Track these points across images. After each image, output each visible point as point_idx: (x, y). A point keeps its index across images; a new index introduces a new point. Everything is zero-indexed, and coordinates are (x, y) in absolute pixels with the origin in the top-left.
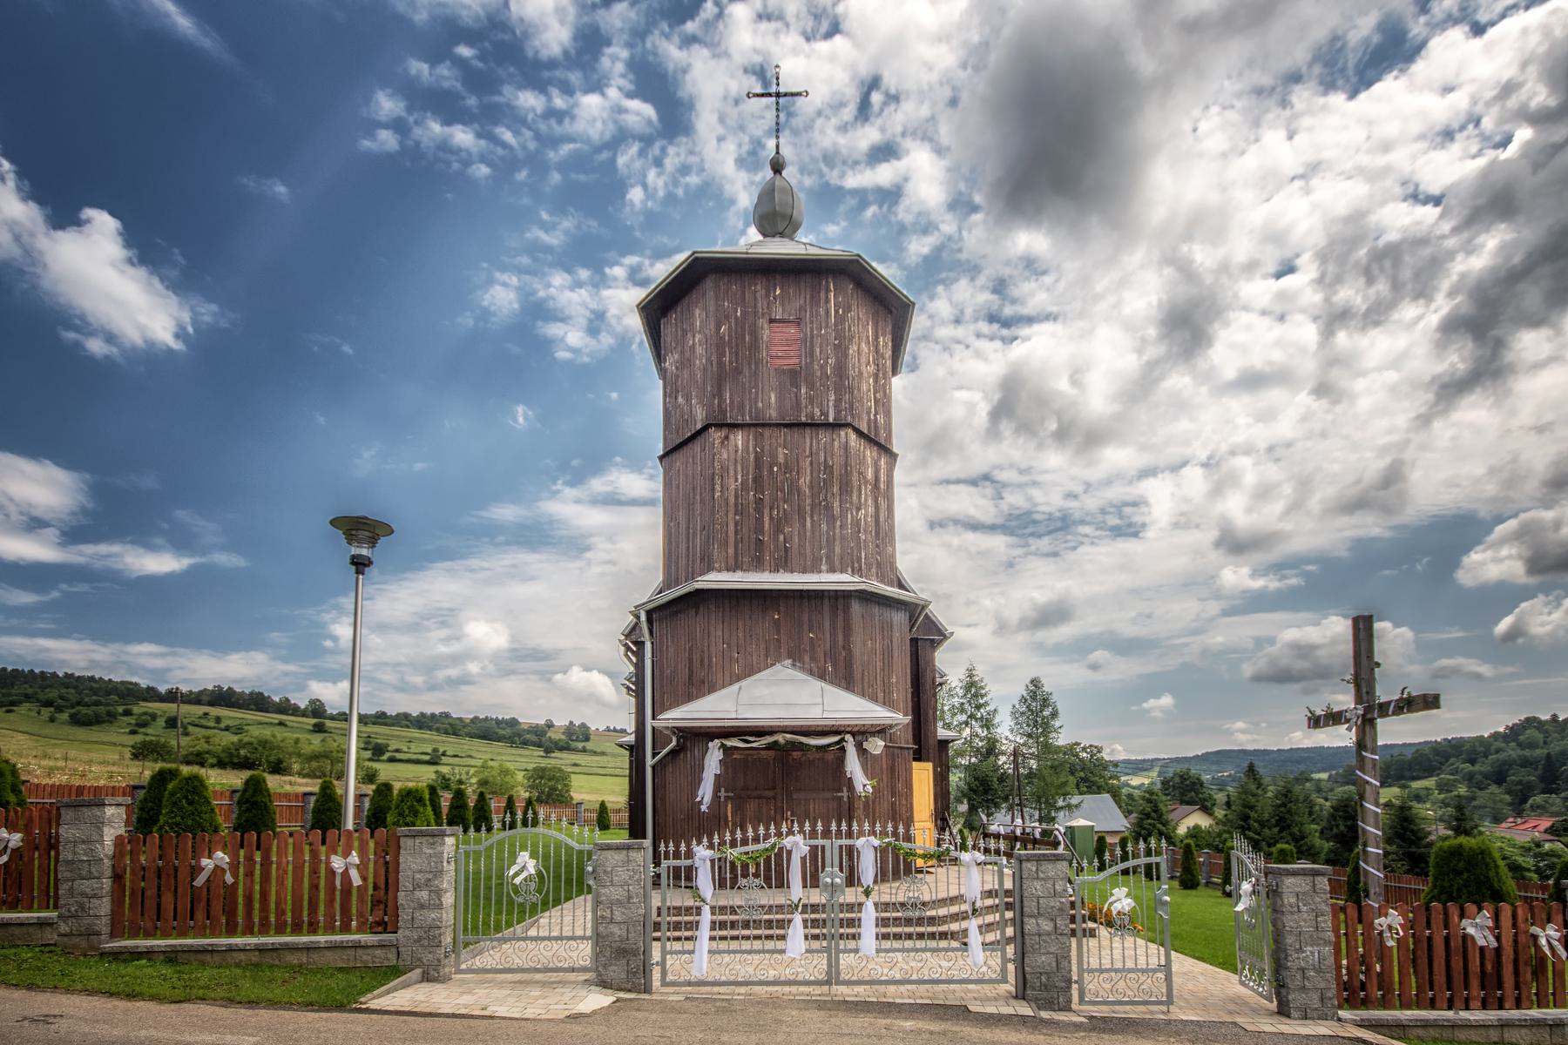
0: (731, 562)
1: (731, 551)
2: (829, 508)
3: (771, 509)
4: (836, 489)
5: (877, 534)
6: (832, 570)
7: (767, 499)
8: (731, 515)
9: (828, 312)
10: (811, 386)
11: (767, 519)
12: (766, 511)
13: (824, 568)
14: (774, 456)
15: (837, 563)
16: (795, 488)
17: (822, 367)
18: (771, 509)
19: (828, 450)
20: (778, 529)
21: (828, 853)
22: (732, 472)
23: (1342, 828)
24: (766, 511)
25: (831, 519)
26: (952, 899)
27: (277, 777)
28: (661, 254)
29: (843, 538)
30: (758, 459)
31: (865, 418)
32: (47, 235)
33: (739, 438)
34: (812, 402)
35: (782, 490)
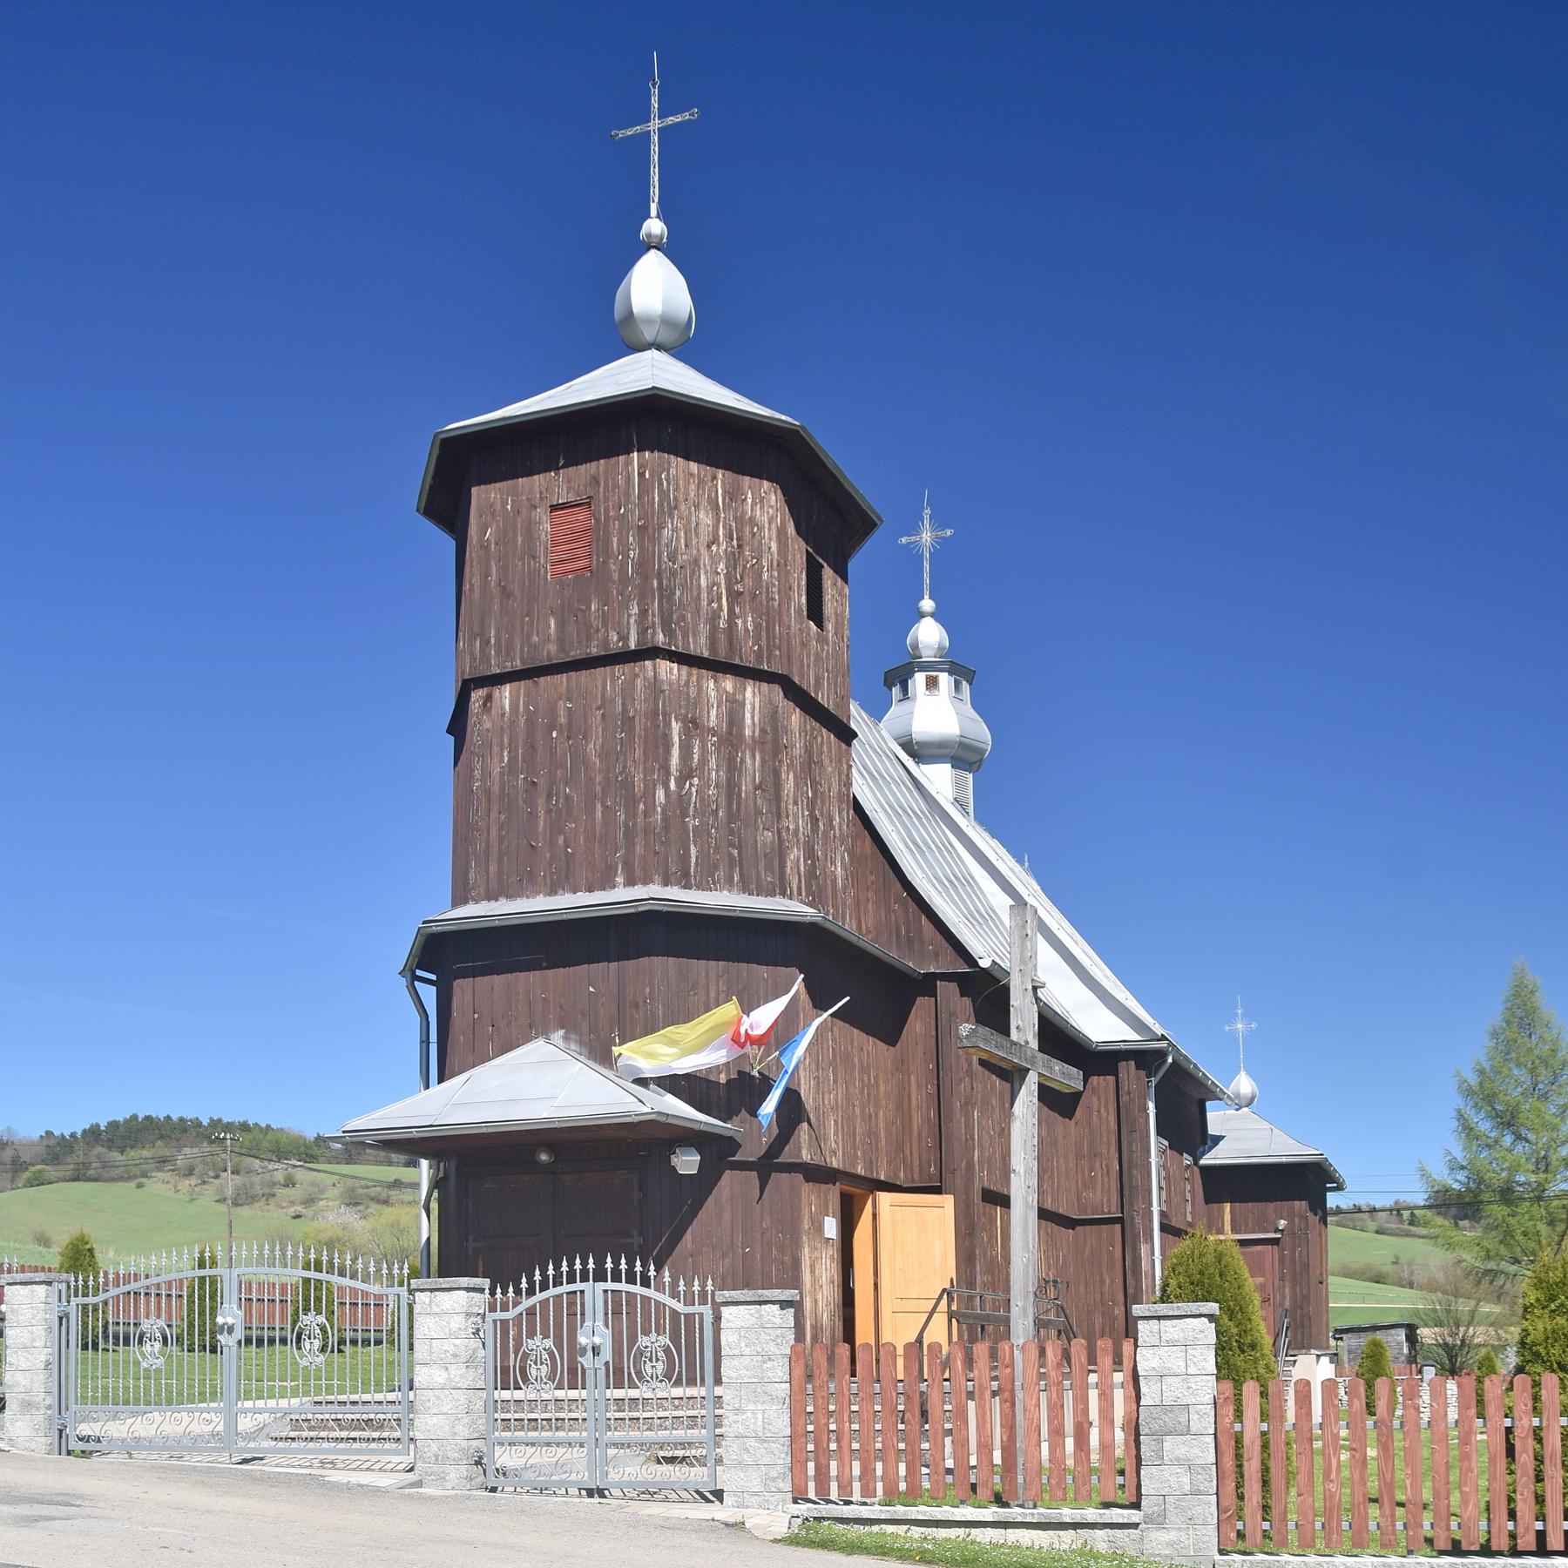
0: (494, 885)
1: (493, 868)
2: (628, 785)
3: (549, 797)
4: (638, 753)
5: (732, 817)
6: (630, 882)
7: (542, 782)
8: (494, 815)
9: (629, 479)
10: (605, 601)
11: (542, 813)
12: (541, 801)
13: (620, 880)
14: (553, 713)
15: (638, 872)
16: (580, 760)
17: (624, 564)
18: (549, 797)
19: (628, 691)
20: (556, 828)
21: (226, 1285)
22: (496, 749)
23: (1480, 1437)
24: (541, 801)
25: (631, 803)
26: (533, 1444)
27: (987, 1354)
28: (809, 628)
29: (648, 831)
30: (531, 722)
31: (704, 630)
32: (1005, 965)
33: (505, 695)
34: (605, 624)
35: (563, 766)
